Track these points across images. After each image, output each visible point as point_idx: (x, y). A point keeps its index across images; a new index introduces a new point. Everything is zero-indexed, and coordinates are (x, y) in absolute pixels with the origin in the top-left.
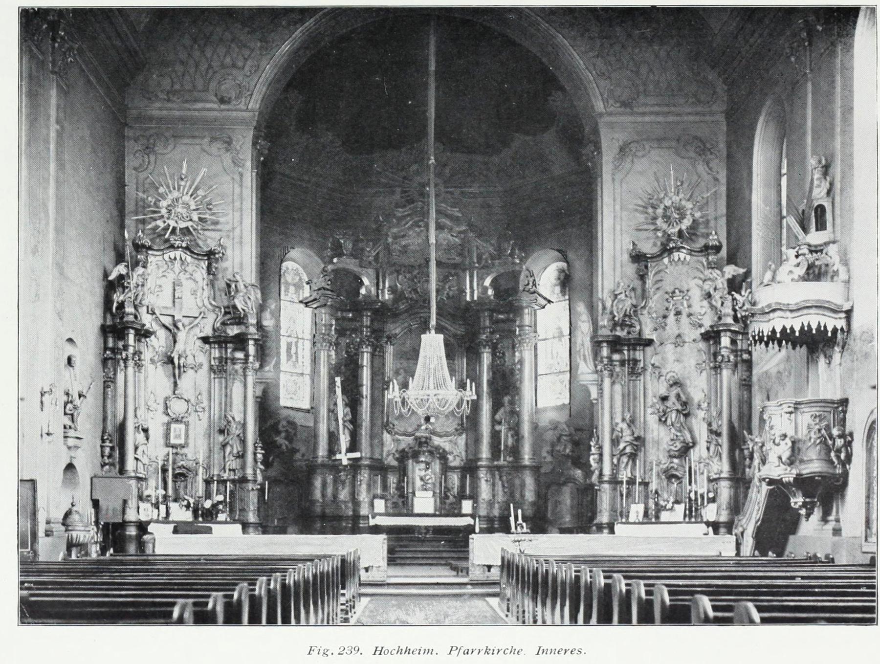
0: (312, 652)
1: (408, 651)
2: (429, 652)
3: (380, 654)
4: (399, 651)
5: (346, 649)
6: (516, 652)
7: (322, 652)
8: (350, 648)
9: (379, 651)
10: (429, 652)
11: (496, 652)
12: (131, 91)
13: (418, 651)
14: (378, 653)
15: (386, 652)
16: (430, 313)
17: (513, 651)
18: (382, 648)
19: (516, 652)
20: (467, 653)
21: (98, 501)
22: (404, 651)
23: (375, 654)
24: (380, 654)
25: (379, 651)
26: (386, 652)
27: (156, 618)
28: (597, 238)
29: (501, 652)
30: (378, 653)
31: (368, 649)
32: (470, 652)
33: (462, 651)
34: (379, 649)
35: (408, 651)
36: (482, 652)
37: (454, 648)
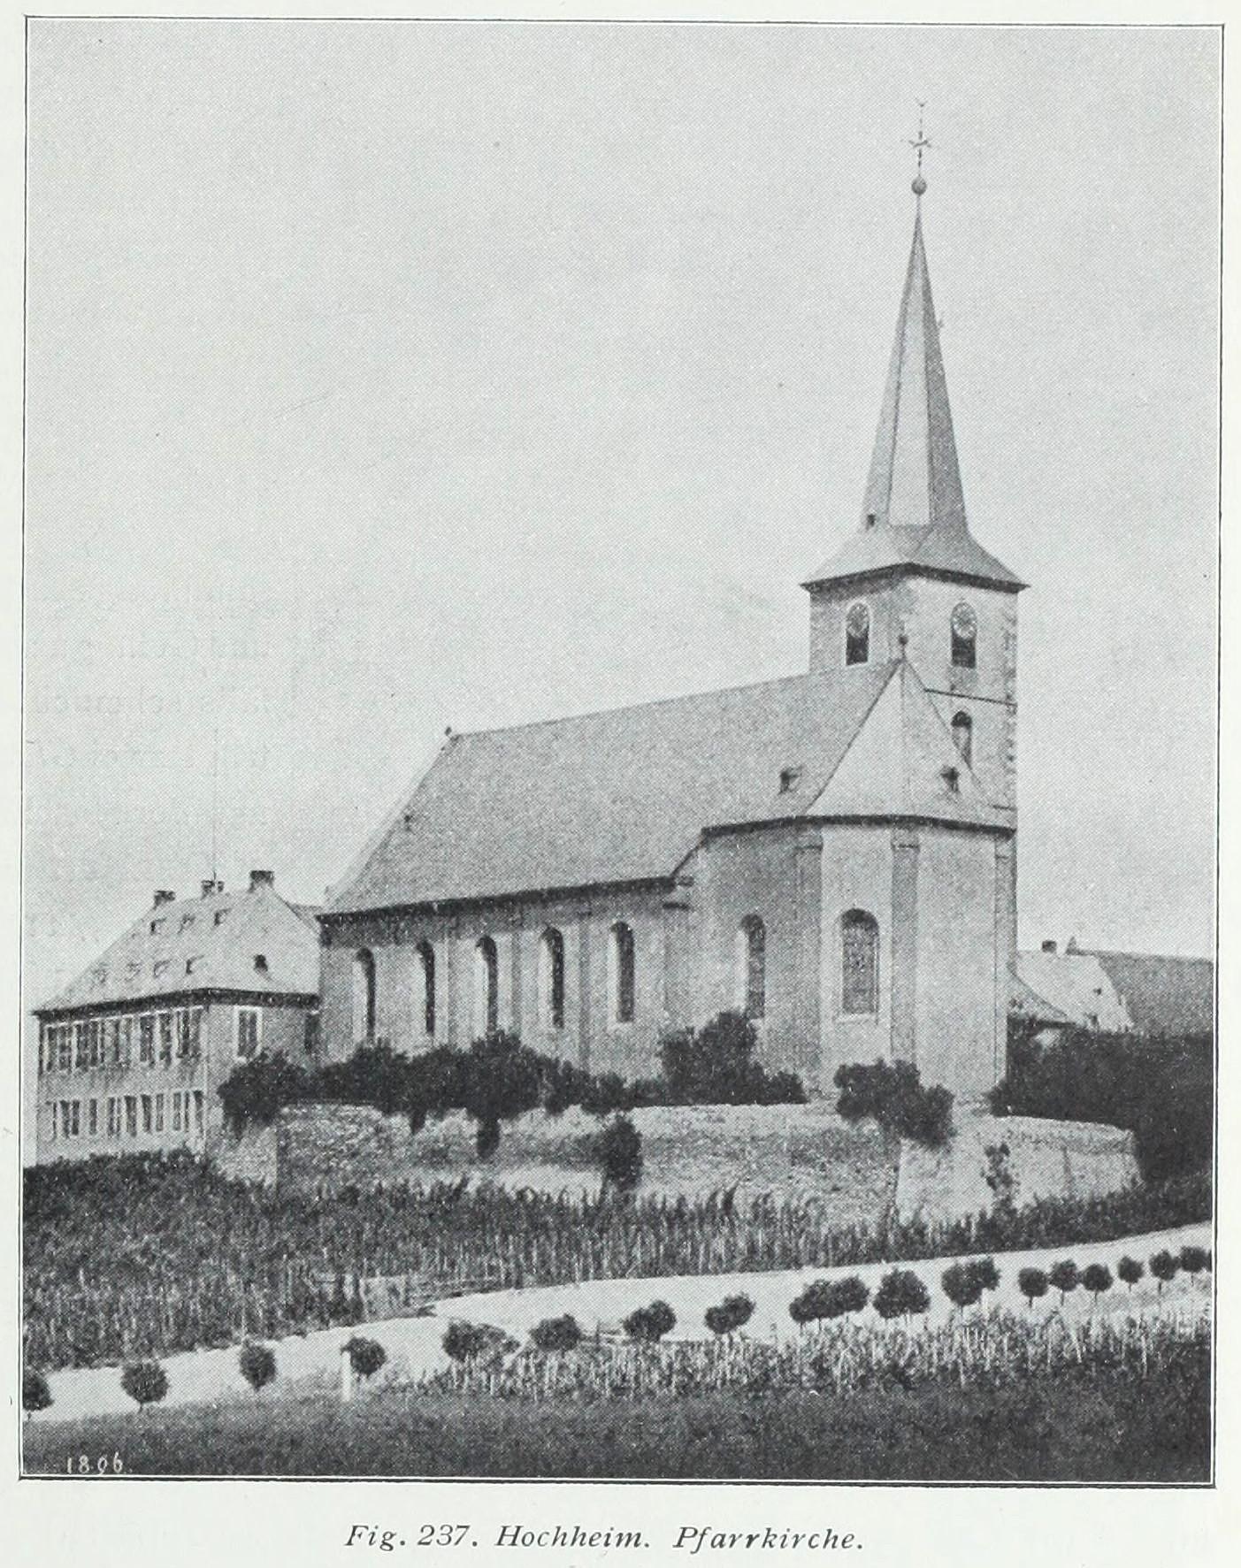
0: (355, 1539)
1: (580, 1537)
2: (634, 1539)
3: (513, 1543)
4: (559, 1538)
5: (437, 1529)
6: (587, 1540)
7: (379, 1539)
8: (447, 1530)
9: (512, 1536)
10: (634, 1539)
11: (790, 1541)
12: (549, 1007)
13: (603, 1539)
14: (507, 1540)
15: (529, 1538)
16: (826, 1265)
17: (831, 1539)
18: (519, 1528)
19: (587, 1540)
20: (721, 1544)
21: (706, 831)
22: (569, 1540)
23: (499, 1543)
24: (513, 1543)
25: (512, 1536)
26: (528, 1540)
27: (624, 973)
28: (24, 1186)
29: (803, 1543)
30: (507, 1540)
31: (660, 1536)
32: (727, 1541)
33: (707, 1540)
34: (511, 1531)
35: (580, 1537)
36: (757, 1543)
37: (689, 1532)
